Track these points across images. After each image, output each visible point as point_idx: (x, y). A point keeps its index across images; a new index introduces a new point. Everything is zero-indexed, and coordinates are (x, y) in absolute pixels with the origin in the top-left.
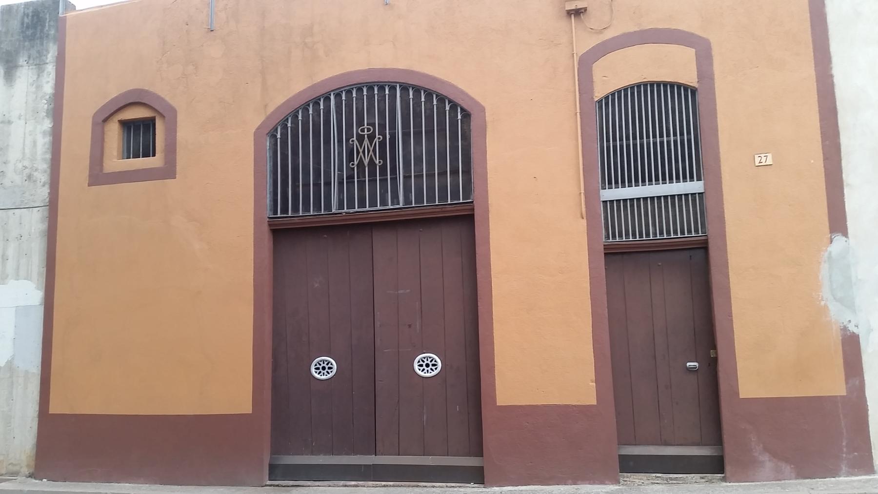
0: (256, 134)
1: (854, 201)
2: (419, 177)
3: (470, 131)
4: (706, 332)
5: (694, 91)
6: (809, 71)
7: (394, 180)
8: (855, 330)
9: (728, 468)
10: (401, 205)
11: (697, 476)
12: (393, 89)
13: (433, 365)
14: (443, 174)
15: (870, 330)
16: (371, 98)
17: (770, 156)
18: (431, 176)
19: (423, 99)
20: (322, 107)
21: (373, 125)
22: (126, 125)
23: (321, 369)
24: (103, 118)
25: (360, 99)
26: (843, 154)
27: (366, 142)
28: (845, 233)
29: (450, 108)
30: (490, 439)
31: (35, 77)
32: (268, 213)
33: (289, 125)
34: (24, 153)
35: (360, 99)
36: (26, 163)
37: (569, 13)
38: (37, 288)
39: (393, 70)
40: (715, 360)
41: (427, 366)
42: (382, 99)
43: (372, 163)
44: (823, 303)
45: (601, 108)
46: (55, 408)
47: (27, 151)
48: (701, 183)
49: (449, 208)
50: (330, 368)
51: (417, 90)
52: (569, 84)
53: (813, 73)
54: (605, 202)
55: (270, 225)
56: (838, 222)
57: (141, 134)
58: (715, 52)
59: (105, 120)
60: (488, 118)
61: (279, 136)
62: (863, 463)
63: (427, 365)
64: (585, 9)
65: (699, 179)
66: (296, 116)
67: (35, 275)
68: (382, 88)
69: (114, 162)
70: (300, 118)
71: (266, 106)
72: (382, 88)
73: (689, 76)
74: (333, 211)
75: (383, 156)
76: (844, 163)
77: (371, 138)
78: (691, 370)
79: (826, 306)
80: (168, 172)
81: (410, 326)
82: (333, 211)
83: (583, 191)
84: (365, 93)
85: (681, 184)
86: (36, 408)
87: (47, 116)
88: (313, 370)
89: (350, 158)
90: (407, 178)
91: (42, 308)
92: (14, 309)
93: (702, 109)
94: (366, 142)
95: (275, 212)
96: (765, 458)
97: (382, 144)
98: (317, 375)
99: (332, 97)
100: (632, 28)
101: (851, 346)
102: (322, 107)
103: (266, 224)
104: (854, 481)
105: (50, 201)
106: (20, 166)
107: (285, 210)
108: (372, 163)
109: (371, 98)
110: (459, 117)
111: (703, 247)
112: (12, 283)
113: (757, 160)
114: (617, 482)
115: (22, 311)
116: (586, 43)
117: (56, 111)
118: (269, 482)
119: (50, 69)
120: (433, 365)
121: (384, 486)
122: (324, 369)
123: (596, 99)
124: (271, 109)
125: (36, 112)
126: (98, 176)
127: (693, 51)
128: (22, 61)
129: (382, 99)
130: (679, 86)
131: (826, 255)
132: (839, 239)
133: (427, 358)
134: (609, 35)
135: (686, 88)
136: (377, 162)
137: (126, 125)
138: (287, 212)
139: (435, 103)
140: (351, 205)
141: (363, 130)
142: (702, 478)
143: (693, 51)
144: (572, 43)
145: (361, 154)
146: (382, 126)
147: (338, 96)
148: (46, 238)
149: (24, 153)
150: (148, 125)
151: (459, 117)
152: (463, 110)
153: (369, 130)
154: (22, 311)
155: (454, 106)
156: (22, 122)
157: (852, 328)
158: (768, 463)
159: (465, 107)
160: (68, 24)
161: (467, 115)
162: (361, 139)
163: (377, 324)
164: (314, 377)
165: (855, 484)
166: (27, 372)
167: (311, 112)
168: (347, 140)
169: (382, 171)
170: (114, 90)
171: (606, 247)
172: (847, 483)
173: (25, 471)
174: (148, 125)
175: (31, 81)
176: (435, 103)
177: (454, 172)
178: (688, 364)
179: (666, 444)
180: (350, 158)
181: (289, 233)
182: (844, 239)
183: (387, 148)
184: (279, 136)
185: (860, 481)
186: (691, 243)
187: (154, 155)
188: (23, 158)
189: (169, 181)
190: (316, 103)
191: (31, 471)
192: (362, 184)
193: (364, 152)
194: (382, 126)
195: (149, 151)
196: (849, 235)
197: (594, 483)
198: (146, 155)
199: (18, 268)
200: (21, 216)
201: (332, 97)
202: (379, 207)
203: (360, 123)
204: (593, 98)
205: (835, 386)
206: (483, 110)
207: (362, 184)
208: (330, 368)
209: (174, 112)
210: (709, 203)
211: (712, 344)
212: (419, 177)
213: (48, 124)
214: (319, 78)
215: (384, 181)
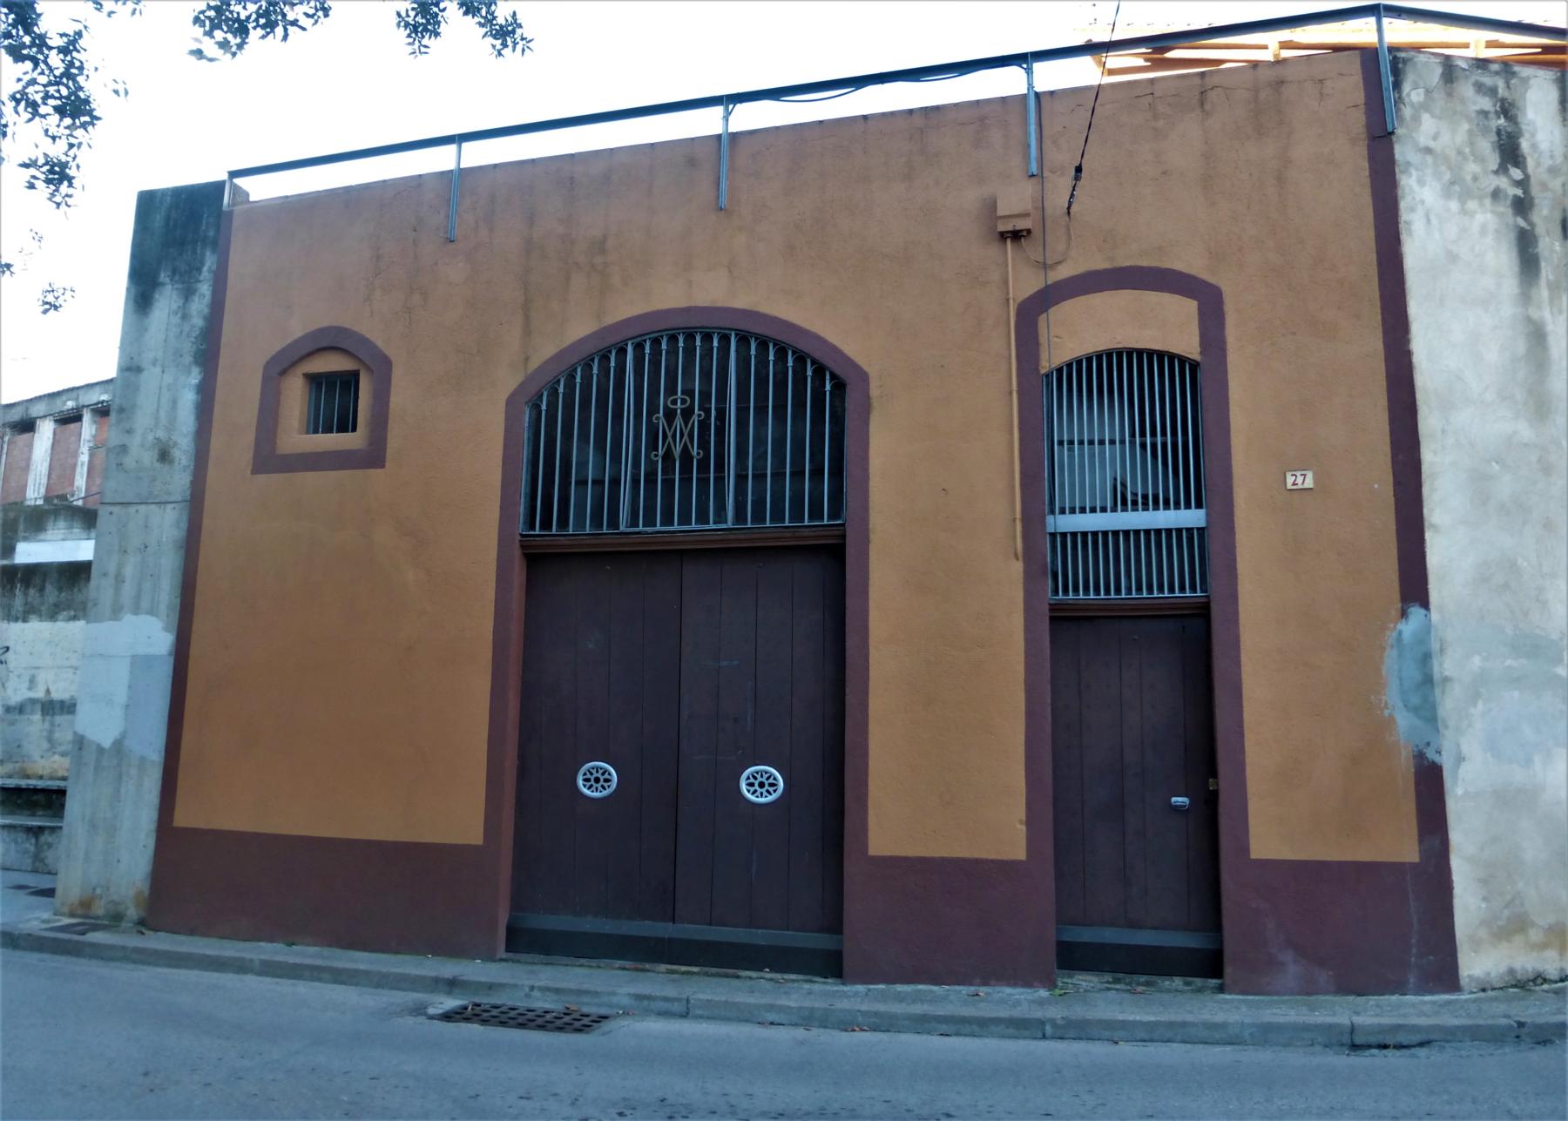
0: (511, 401)
1: (1444, 551)
2: (760, 477)
3: (844, 410)
4: (1201, 748)
5: (1195, 366)
6: (1374, 343)
7: (720, 480)
8: (1436, 758)
9: (1228, 970)
10: (730, 525)
11: (1178, 982)
12: (725, 339)
13: (771, 785)
14: (798, 474)
15: (1460, 759)
16: (689, 351)
17: (1310, 475)
18: (778, 475)
19: (771, 357)
20: (612, 364)
21: (691, 393)
22: (315, 380)
23: (595, 781)
24: (279, 367)
25: (673, 352)
26: (1424, 476)
27: (679, 421)
28: (1425, 604)
29: (814, 372)
30: (854, 910)
31: (181, 302)
32: (520, 527)
33: (561, 390)
34: (157, 419)
35: (673, 352)
36: (161, 434)
37: (1003, 236)
38: (166, 629)
39: (727, 310)
40: (1214, 796)
41: (762, 784)
42: (707, 354)
43: (686, 452)
44: (1386, 712)
45: (1050, 385)
46: (181, 819)
47: (162, 414)
48: (1201, 513)
49: (806, 532)
50: (606, 780)
51: (763, 344)
52: (1001, 344)
53: (1380, 346)
54: (1053, 535)
55: (522, 547)
56: (1414, 586)
57: (336, 400)
58: (1229, 307)
59: (283, 372)
60: (874, 392)
61: (544, 407)
62: (383, 466)
63: (762, 785)
64: (1029, 231)
65: (1199, 506)
66: (572, 377)
67: (163, 608)
68: (707, 337)
69: (295, 438)
70: (578, 380)
71: (527, 359)
72: (707, 337)
73: (1187, 344)
74: (622, 528)
75: (704, 444)
76: (1426, 490)
77: (688, 413)
78: (1177, 809)
79: (1392, 719)
80: (374, 457)
81: (736, 720)
82: (622, 528)
83: (1018, 516)
84: (681, 344)
85: (1172, 513)
86: (154, 815)
87: (196, 363)
88: (580, 782)
89: (653, 445)
90: (741, 478)
91: (171, 660)
92: (128, 660)
93: (1206, 392)
94: (679, 421)
95: (533, 527)
96: (1287, 956)
97: (704, 425)
98: (586, 791)
99: (630, 349)
100: (1100, 263)
101: (1429, 783)
102: (612, 364)
103: (517, 545)
104: (1425, 1003)
105: (192, 495)
106: (150, 437)
107: (546, 524)
108: (686, 452)
109: (689, 351)
110: (828, 387)
111: (1202, 612)
112: (128, 618)
113: (1290, 480)
114: (1051, 985)
115: (140, 663)
116: (1027, 284)
117: (208, 352)
118: (504, 956)
119: (205, 289)
120: (771, 785)
121: (683, 973)
122: (597, 780)
123: (1043, 371)
124: (534, 364)
125: (178, 354)
126: (268, 459)
127: (1194, 304)
128: (163, 277)
129: (707, 354)
130: (1172, 357)
131: (1394, 635)
132: (1416, 612)
133: (762, 773)
134: (1064, 272)
135: (1183, 360)
136: (695, 453)
137: (315, 380)
138: (550, 528)
139: (790, 363)
140: (650, 521)
141: (674, 402)
142: (1187, 984)
143: (1194, 304)
144: (1006, 282)
145: (670, 439)
146: (705, 396)
147: (639, 347)
148: (182, 552)
149: (157, 419)
150: (348, 382)
151: (828, 387)
152: (833, 376)
153: (684, 402)
154: (140, 663)
155: (820, 370)
156: (158, 370)
157: (1431, 755)
158: (1293, 969)
159: (838, 371)
160: (236, 223)
161: (840, 386)
162: (670, 415)
163: (685, 714)
164: (582, 794)
165: (1425, 1008)
166: (143, 759)
167: (595, 371)
168: (650, 414)
169: (700, 467)
170: (298, 328)
171: (1053, 607)
172: (1413, 1005)
173: (132, 913)
174: (348, 382)
175: (174, 306)
176: (790, 363)
177: (817, 472)
178: (1174, 799)
179: (1134, 925)
180: (653, 445)
181: (545, 559)
182: (1423, 611)
183: (711, 432)
184: (544, 407)
185: (1434, 1003)
186: (1160, 607)
187: (354, 430)
188: (156, 425)
189: (379, 471)
190: (605, 358)
191: (143, 914)
192: (669, 484)
193: (674, 436)
194: (705, 396)
195: (346, 423)
196: (1432, 607)
197: (1015, 985)
198: (342, 428)
199: (138, 597)
200: (147, 517)
201: (630, 349)
202: (694, 526)
203: (671, 390)
204: (1037, 369)
205: (1400, 845)
206: (864, 377)
207: (669, 484)
208: (606, 780)
209: (387, 363)
210: (1215, 547)
211: (1210, 766)
212: (760, 477)
213: (195, 377)
214: (611, 319)
215: (704, 482)
